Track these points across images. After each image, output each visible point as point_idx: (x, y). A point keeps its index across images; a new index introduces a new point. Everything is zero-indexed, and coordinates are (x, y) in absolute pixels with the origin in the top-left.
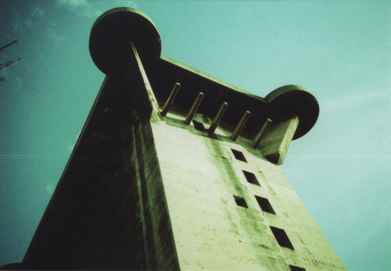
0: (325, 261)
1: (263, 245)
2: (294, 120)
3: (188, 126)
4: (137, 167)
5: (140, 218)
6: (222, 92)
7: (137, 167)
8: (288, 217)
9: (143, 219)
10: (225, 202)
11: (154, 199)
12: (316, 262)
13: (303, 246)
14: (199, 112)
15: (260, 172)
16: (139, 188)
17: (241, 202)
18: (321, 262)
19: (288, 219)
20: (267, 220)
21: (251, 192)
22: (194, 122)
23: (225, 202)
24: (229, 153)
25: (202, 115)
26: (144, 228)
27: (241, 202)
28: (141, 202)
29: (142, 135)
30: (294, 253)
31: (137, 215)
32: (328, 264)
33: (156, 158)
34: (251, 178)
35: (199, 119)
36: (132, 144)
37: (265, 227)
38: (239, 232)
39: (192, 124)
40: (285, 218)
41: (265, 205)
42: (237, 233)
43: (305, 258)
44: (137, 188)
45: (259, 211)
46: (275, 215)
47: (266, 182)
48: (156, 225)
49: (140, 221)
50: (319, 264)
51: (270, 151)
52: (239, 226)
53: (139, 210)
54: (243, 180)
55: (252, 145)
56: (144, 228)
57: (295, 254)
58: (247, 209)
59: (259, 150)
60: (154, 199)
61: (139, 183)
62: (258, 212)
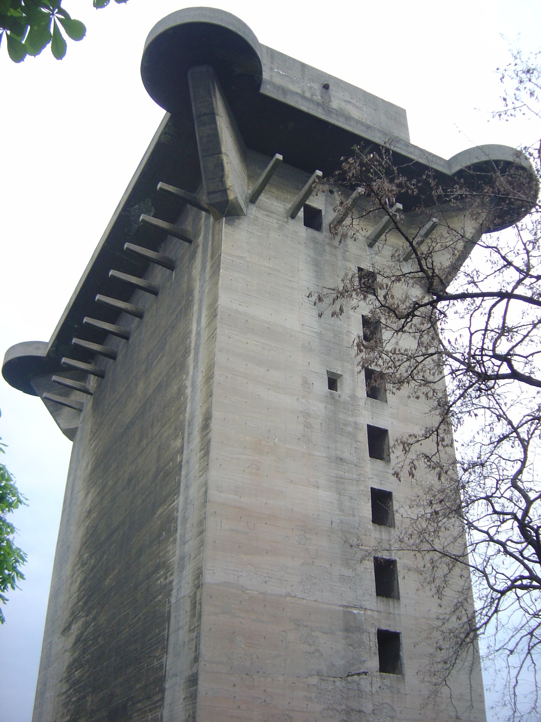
44: (191, 331)
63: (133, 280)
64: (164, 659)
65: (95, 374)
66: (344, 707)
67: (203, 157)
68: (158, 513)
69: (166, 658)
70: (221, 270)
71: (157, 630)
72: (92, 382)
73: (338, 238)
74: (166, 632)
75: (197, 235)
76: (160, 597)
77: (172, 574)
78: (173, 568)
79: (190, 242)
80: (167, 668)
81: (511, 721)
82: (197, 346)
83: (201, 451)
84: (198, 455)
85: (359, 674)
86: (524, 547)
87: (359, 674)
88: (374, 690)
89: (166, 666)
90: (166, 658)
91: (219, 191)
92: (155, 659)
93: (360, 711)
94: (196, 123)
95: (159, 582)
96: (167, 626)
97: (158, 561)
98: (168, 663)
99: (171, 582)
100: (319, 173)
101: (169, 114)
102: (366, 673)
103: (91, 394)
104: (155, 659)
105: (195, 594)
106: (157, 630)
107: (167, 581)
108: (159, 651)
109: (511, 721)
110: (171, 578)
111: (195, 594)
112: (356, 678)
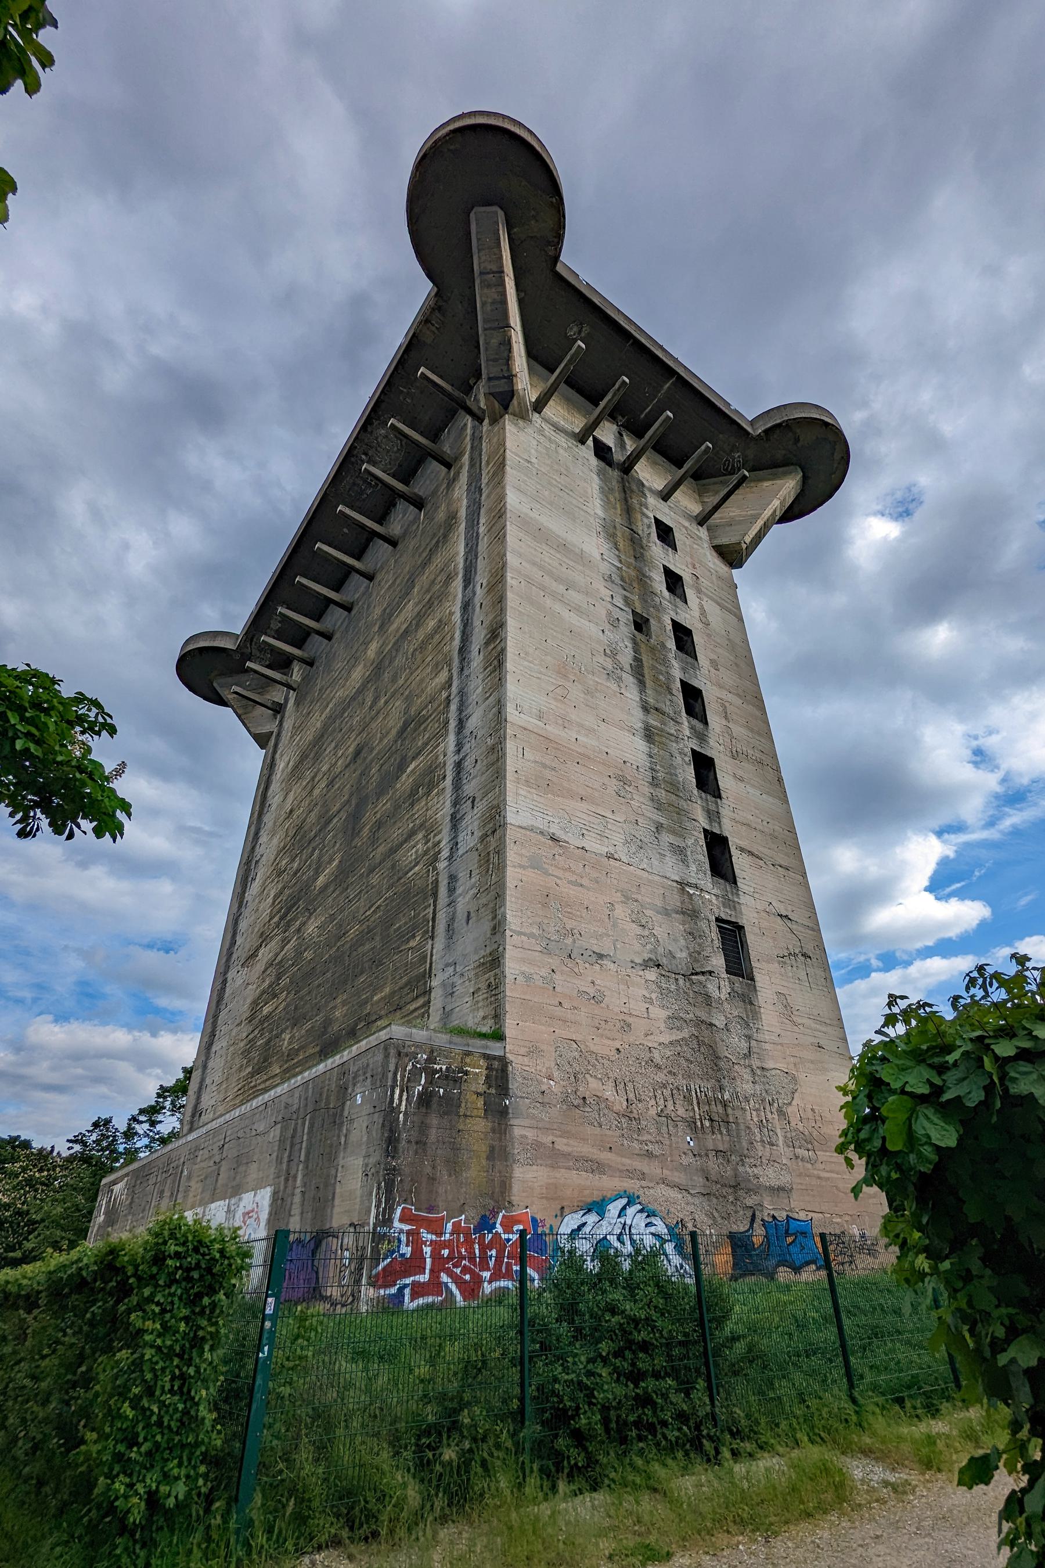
3: (583, 447)
4: (463, 513)
13: (724, 722)
22: (596, 441)
39: (590, 442)
40: (712, 669)
43: (721, 742)
44: (457, 554)
63: (369, 523)
65: (302, 660)
66: (691, 1015)
67: (485, 329)
68: (409, 769)
70: (507, 467)
72: (297, 673)
75: (458, 458)
77: (440, 832)
79: (448, 466)
81: (10, 976)
84: (481, 677)
85: (703, 973)
87: (703, 973)
88: (723, 997)
89: (432, 955)
91: (504, 377)
93: (711, 1025)
94: (477, 282)
96: (432, 901)
97: (411, 825)
98: (434, 951)
101: (436, 289)
102: (711, 973)
103: (294, 690)
107: (430, 844)
108: (418, 938)
109: (10, 976)
110: (437, 839)
112: (700, 977)
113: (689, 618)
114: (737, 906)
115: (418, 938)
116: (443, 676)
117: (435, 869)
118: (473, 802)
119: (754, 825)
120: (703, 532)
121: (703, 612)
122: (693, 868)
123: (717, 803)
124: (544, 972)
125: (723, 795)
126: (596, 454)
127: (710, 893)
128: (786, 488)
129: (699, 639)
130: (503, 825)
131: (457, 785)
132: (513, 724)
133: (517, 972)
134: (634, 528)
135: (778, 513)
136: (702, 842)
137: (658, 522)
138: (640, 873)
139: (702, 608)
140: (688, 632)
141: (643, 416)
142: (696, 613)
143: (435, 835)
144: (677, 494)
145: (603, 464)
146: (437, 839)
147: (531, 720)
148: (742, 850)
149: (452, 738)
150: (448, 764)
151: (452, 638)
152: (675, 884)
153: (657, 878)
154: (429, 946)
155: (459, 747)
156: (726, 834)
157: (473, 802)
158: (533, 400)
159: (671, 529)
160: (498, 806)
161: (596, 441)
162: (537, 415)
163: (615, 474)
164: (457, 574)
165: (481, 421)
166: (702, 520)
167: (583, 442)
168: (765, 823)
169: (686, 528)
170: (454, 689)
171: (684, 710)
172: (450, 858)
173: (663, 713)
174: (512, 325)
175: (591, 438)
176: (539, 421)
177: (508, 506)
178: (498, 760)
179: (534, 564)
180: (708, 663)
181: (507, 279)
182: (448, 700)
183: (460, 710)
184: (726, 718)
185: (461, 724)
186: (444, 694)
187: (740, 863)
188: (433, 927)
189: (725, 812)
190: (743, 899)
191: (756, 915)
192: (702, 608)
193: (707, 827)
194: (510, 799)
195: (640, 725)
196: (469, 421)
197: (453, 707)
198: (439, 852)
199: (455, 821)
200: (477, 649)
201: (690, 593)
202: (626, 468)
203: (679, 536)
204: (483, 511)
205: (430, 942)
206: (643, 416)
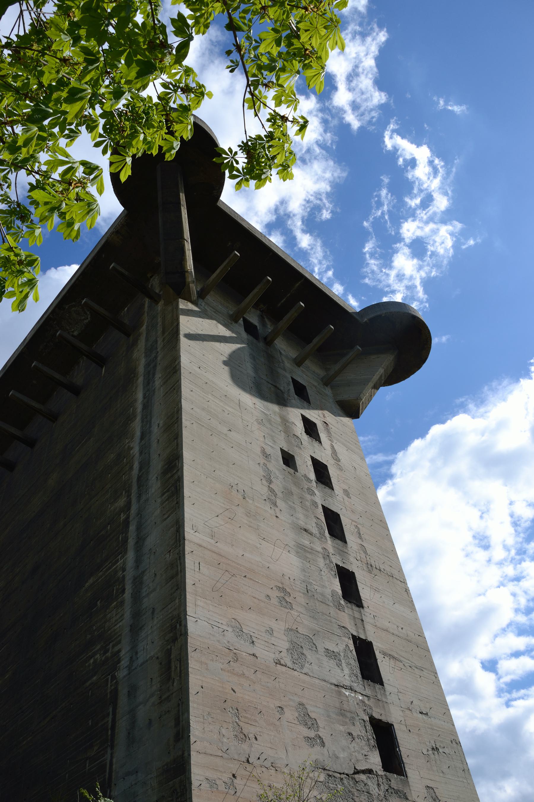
0: (382, 567)
1: (307, 529)
2: (435, 202)
3: (236, 325)
4: (141, 369)
5: (130, 449)
6: (298, 284)
7: (141, 369)
8: (348, 497)
9: (136, 450)
10: (267, 456)
11: (161, 425)
12: (371, 566)
13: (359, 541)
14: (256, 306)
15: (325, 423)
16: (140, 402)
17: (288, 460)
18: (378, 568)
19: (349, 500)
20: (319, 496)
21: (306, 452)
22: (246, 321)
23: (267, 456)
24: (288, 384)
25: (258, 312)
26: (136, 466)
27: (288, 460)
28: (137, 426)
29: (159, 320)
30: (432, 461)
31: (127, 442)
32: (385, 572)
33: (177, 363)
34: (311, 428)
35: (254, 319)
36: (141, 331)
37: (315, 504)
38: (277, 504)
39: (241, 321)
40: (345, 498)
41: (321, 472)
42: (275, 505)
43: (358, 558)
44: (136, 400)
45: (311, 481)
46: (332, 491)
47: (330, 440)
48: (157, 465)
49: (132, 452)
50: (374, 569)
51: (347, 395)
52: (280, 494)
53: (133, 437)
54: (299, 428)
55: (322, 379)
56: (136, 466)
57: (346, 551)
58: (296, 472)
59: (332, 388)
60: (161, 425)
61: (140, 396)
62: (309, 480)
64: (108, 756)
69: (112, 754)
71: (90, 721)
73: (510, 571)
74: (110, 719)
76: (95, 678)
77: (119, 642)
78: (120, 635)
79: (128, 335)
80: (114, 767)
82: (147, 406)
83: (163, 495)
84: (159, 500)
86: (341, 45)
90: (112, 754)
92: (88, 762)
95: (92, 661)
96: (111, 710)
97: (89, 637)
99: (120, 651)
100: (326, 215)
101: (126, 211)
104: (88, 762)
105: (169, 653)
106: (90, 721)
107: (109, 654)
108: (96, 748)
110: (116, 649)
111: (169, 653)
113: (325, 457)
114: (385, 705)
115: (96, 748)
116: (121, 502)
117: (114, 677)
118: (153, 613)
119: (391, 631)
120: (328, 391)
121: (334, 452)
122: (347, 671)
123: (360, 612)
124: (226, 777)
125: (365, 604)
126: (246, 330)
127: (358, 695)
128: (385, 362)
129: (333, 472)
130: (185, 634)
131: (137, 597)
132: (190, 542)
133: (202, 778)
134: (278, 385)
135: (383, 378)
136: (352, 647)
137: (295, 382)
138: (303, 677)
139: (333, 447)
140: (325, 467)
141: (279, 305)
142: (329, 451)
143: (113, 647)
144: (307, 362)
145: (251, 338)
146: (116, 649)
147: (205, 538)
148: (385, 654)
149: (131, 555)
150: (127, 578)
151: (131, 468)
152: (333, 687)
153: (317, 681)
154: (108, 756)
155: (138, 561)
156: (369, 639)
157: (153, 613)
158: (198, 290)
159: (304, 387)
160: (179, 615)
161: (246, 321)
162: (202, 300)
163: (261, 345)
164: (135, 417)
165: (157, 302)
166: (327, 382)
167: (236, 321)
168: (400, 629)
169: (315, 387)
170: (134, 510)
171: (327, 531)
172: (129, 667)
173: (311, 534)
174: (185, 238)
175: (242, 319)
176: (203, 304)
177: (182, 365)
178: (177, 574)
179: (203, 409)
180: (342, 492)
181: (182, 208)
182: (127, 523)
183: (139, 528)
184: (360, 537)
185: (140, 541)
186: (123, 517)
187: (385, 666)
188: (113, 735)
189: (367, 619)
190: (391, 699)
191: (401, 713)
192: (333, 447)
193: (355, 634)
194: (190, 610)
195: (294, 543)
196: (147, 301)
197: (132, 528)
198: (119, 661)
199: (135, 629)
200: (154, 478)
201: (323, 436)
202: (268, 341)
203: (310, 392)
204: (159, 368)
205: (109, 751)
206: (279, 305)
